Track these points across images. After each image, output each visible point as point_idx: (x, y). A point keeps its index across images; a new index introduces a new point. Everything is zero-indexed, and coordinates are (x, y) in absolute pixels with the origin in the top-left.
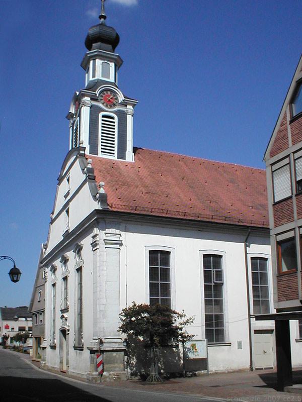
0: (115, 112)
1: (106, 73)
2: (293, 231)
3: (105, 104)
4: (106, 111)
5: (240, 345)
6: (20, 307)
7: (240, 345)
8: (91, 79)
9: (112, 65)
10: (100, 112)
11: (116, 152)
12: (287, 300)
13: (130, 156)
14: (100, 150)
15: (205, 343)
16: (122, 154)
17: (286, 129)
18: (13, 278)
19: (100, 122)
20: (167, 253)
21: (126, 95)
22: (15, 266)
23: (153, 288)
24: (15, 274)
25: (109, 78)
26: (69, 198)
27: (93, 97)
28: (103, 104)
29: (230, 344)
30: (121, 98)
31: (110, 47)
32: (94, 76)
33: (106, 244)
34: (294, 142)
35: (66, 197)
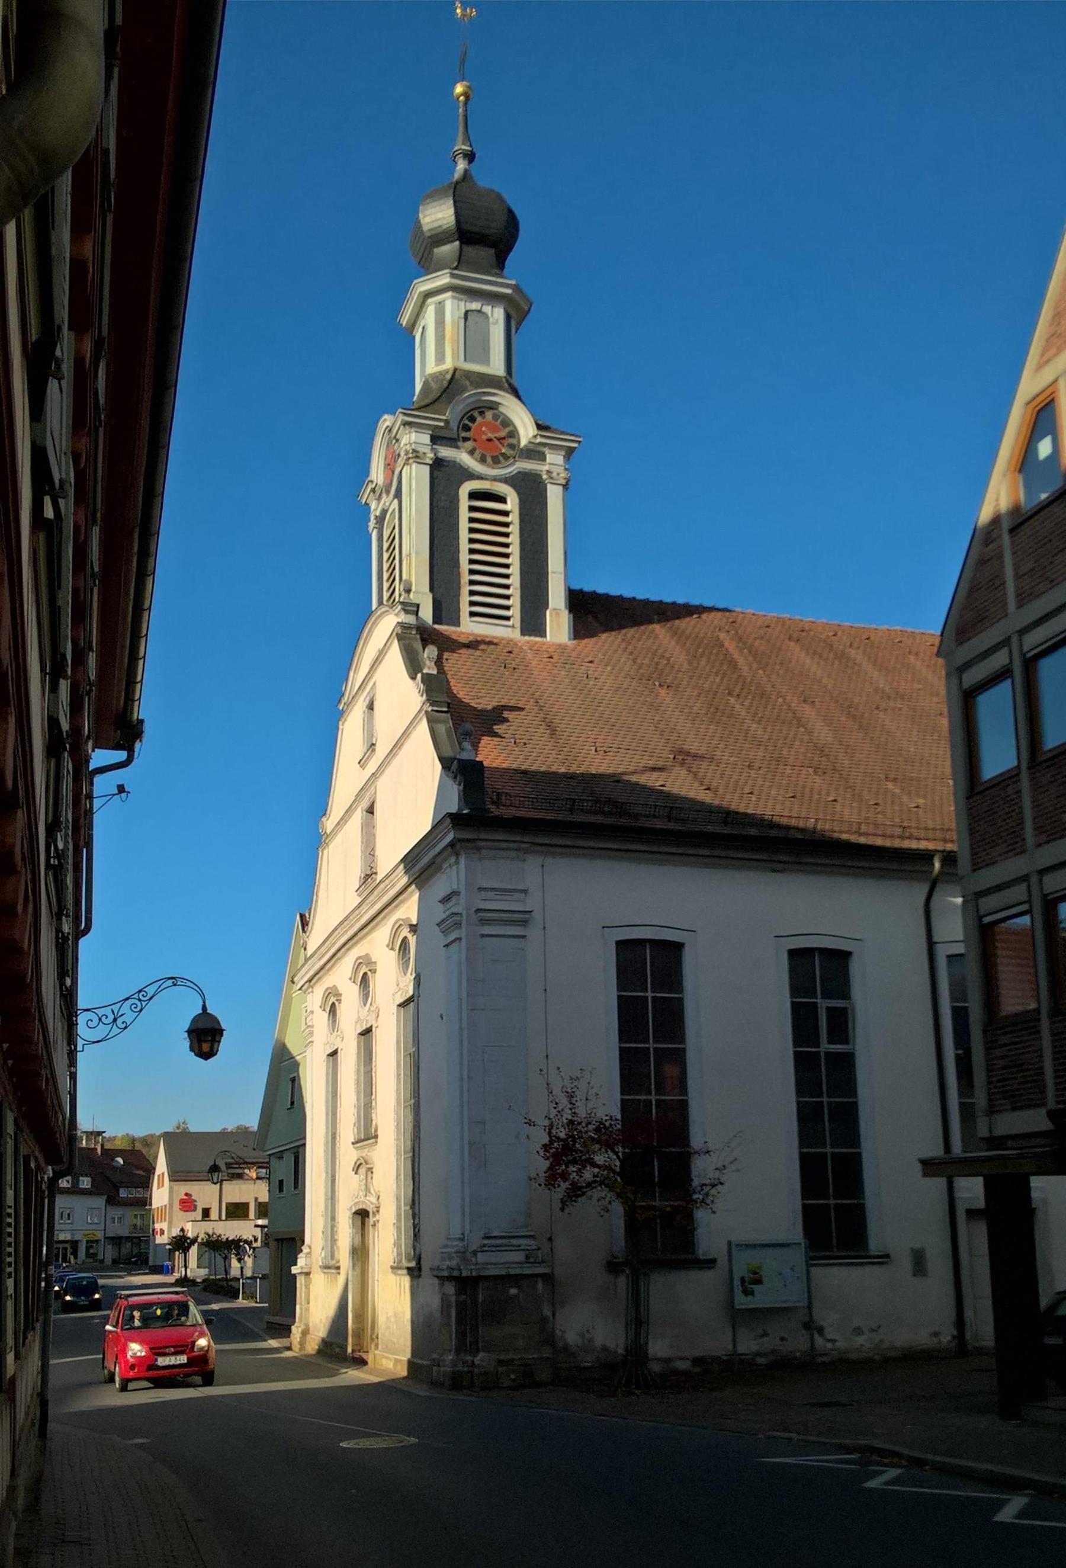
0: (506, 480)
1: (473, 341)
2: (1024, 886)
3: (477, 454)
4: (480, 477)
5: (919, 1263)
6: (432, 589)
7: (919, 1263)
8: (432, 368)
9: (497, 314)
10: (461, 483)
11: (515, 612)
12: (1014, 1109)
13: (558, 624)
14: (465, 609)
15: (798, 1257)
16: (533, 624)
17: (1000, 557)
18: (200, 1047)
19: (464, 514)
20: (675, 948)
21: (540, 422)
22: (204, 1008)
23: (632, 1065)
24: (205, 1036)
25: (486, 361)
26: (372, 766)
27: (441, 433)
28: (471, 453)
29: (884, 1258)
30: (526, 431)
31: (487, 254)
32: (440, 357)
33: (483, 922)
34: (1022, 600)
35: (363, 763)
